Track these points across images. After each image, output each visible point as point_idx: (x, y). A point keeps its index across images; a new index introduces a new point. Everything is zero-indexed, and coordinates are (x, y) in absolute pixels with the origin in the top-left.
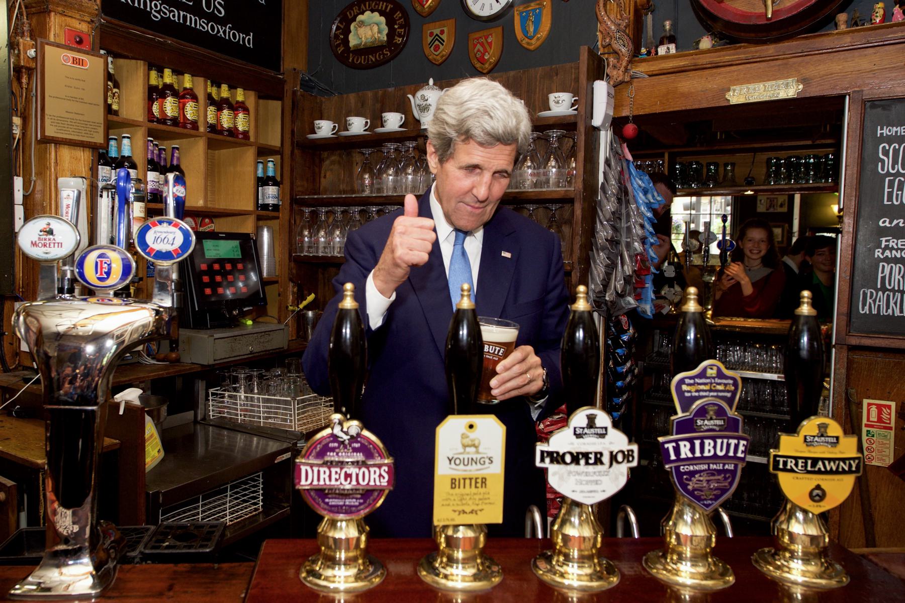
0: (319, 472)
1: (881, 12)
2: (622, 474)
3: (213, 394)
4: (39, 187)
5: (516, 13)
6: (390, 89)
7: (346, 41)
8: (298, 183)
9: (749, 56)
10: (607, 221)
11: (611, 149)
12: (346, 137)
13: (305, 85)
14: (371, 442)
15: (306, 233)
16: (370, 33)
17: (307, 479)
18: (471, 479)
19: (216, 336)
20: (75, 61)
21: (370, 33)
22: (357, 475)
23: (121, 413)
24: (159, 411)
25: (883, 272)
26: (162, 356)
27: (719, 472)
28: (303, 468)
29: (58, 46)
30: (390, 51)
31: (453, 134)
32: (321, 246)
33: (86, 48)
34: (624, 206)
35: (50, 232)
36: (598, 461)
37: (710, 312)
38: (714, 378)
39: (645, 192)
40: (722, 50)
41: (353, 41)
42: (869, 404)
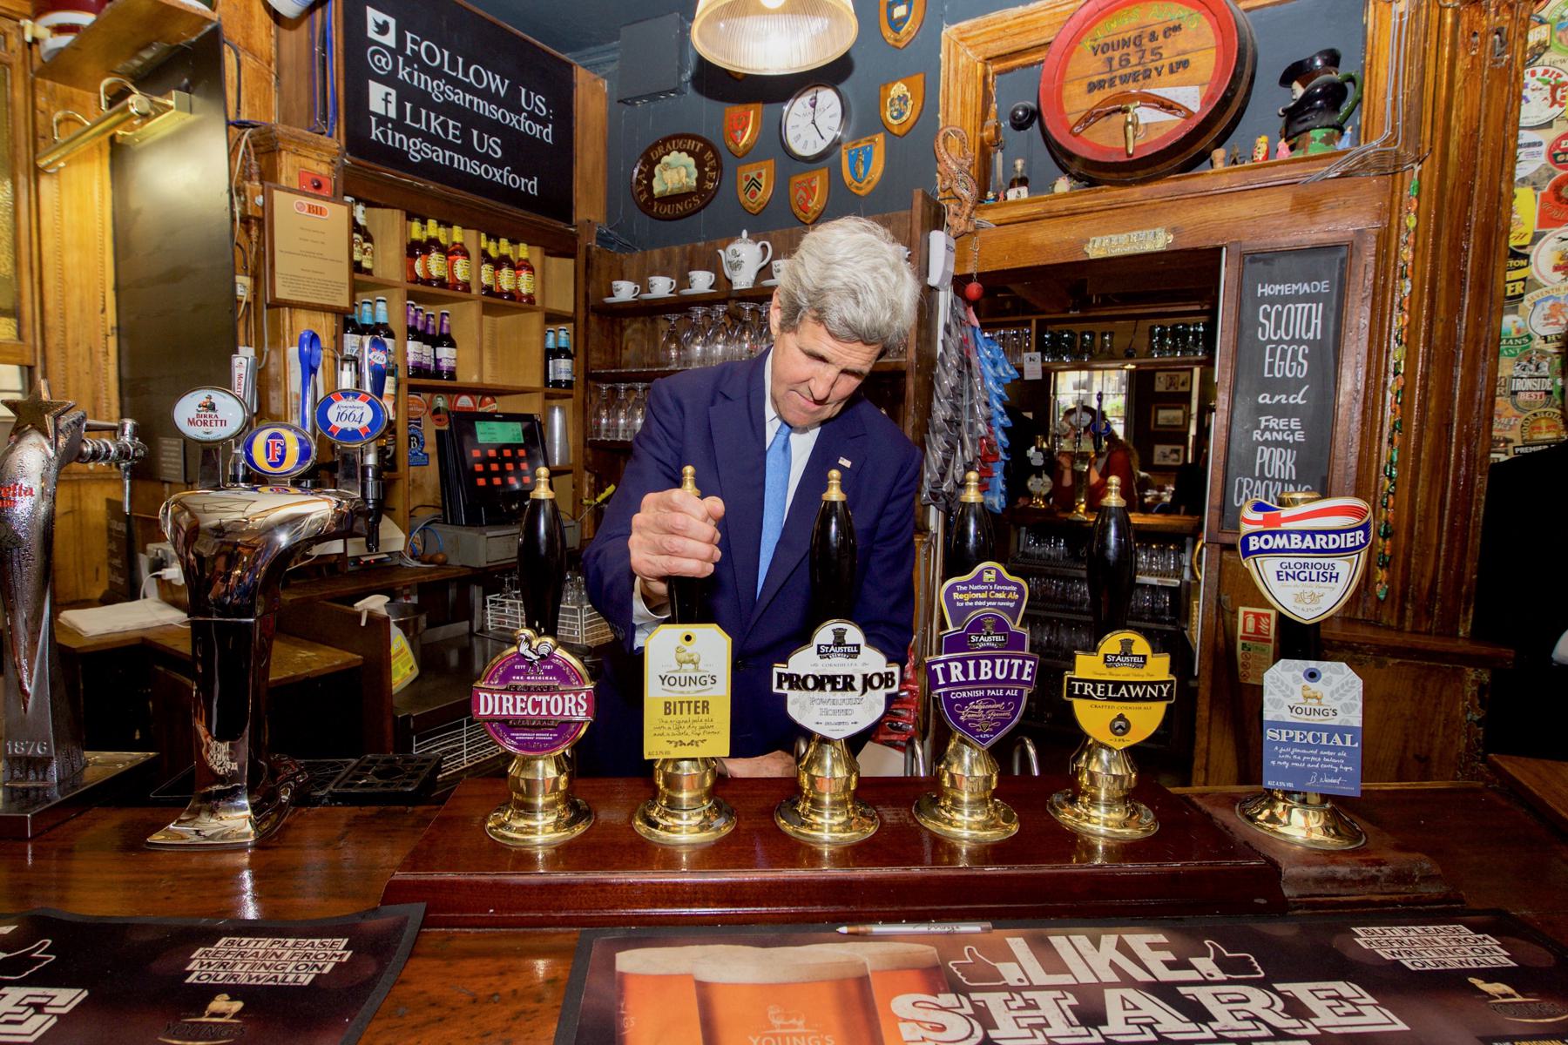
0: (501, 699)
1: (1264, 148)
2: (879, 702)
3: (491, 602)
4: (273, 359)
5: (844, 151)
6: (699, 244)
7: (650, 187)
8: (594, 354)
9: (1113, 200)
10: (946, 398)
11: (952, 313)
12: (647, 301)
13: (602, 239)
14: (567, 664)
15: (604, 413)
16: (677, 177)
17: (486, 710)
18: (689, 703)
19: (489, 534)
20: (311, 209)
21: (677, 177)
22: (548, 703)
23: (363, 624)
24: (416, 621)
25: (1261, 458)
26: (427, 558)
27: (999, 699)
28: (482, 695)
29: (290, 190)
30: (701, 199)
31: (804, 301)
32: (621, 429)
33: (326, 193)
34: (966, 381)
35: (212, 407)
36: (848, 684)
37: (1083, 506)
38: (992, 584)
39: (994, 364)
40: (1080, 193)
41: (658, 187)
42: (1246, 613)
